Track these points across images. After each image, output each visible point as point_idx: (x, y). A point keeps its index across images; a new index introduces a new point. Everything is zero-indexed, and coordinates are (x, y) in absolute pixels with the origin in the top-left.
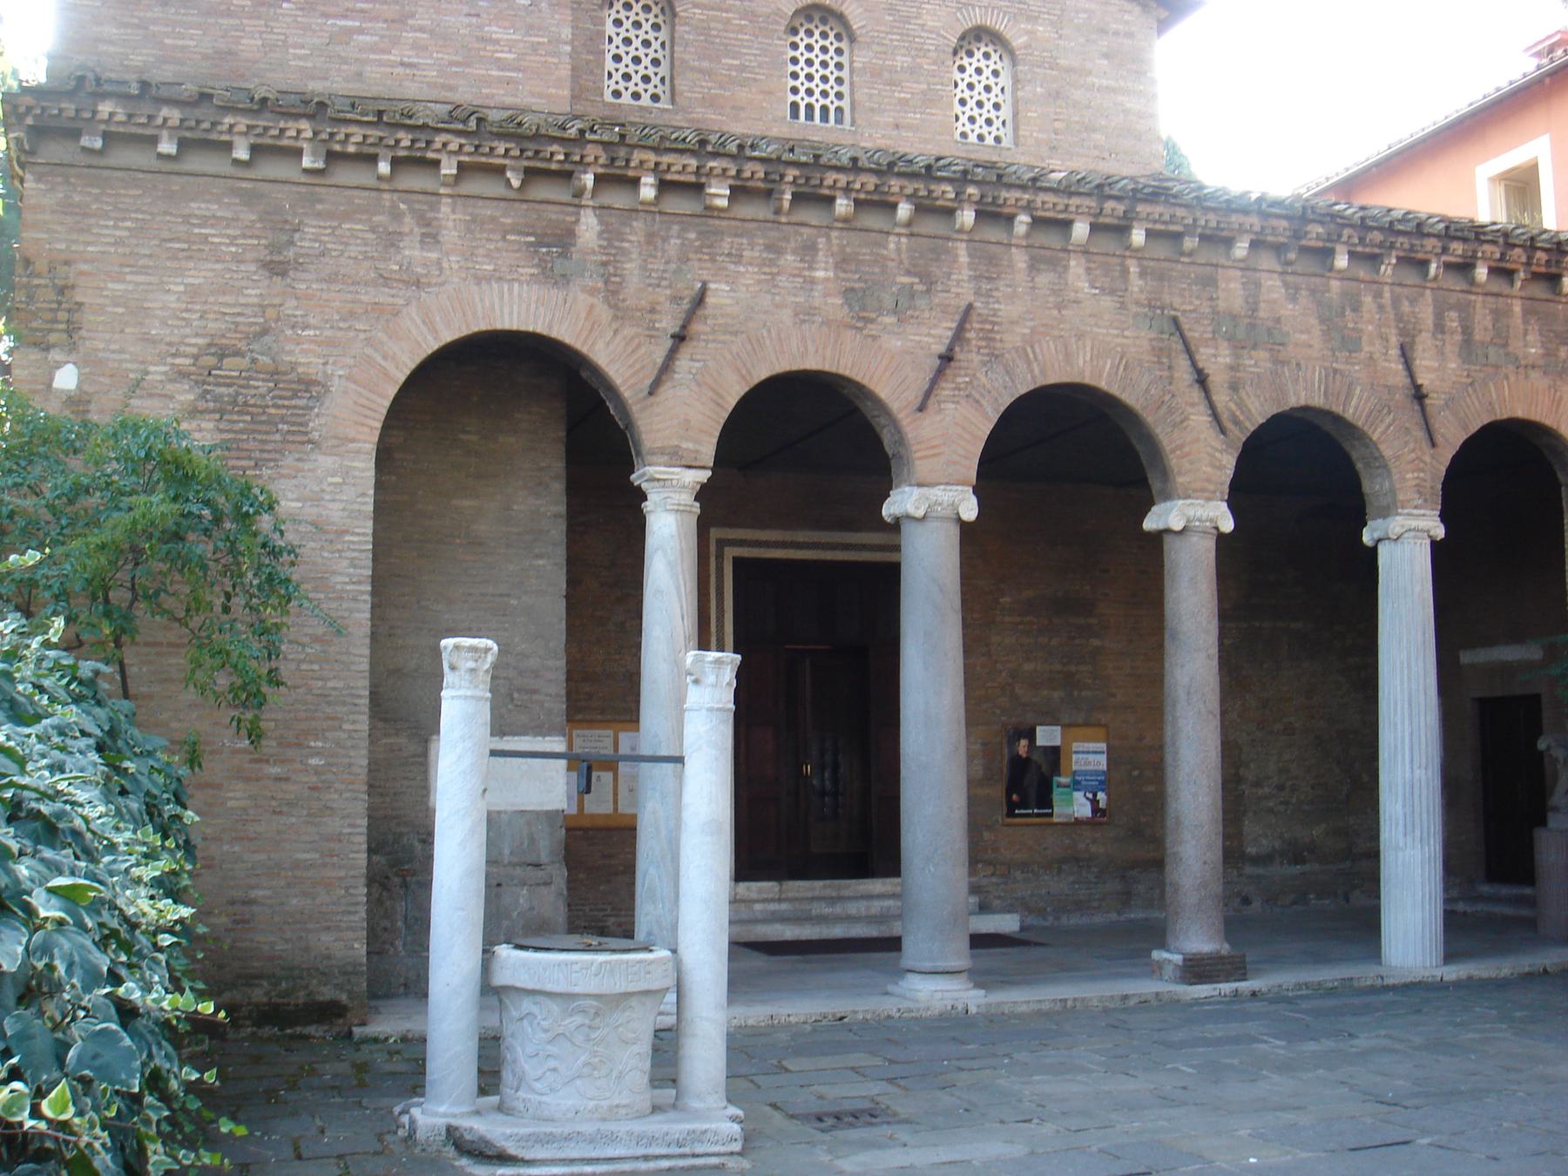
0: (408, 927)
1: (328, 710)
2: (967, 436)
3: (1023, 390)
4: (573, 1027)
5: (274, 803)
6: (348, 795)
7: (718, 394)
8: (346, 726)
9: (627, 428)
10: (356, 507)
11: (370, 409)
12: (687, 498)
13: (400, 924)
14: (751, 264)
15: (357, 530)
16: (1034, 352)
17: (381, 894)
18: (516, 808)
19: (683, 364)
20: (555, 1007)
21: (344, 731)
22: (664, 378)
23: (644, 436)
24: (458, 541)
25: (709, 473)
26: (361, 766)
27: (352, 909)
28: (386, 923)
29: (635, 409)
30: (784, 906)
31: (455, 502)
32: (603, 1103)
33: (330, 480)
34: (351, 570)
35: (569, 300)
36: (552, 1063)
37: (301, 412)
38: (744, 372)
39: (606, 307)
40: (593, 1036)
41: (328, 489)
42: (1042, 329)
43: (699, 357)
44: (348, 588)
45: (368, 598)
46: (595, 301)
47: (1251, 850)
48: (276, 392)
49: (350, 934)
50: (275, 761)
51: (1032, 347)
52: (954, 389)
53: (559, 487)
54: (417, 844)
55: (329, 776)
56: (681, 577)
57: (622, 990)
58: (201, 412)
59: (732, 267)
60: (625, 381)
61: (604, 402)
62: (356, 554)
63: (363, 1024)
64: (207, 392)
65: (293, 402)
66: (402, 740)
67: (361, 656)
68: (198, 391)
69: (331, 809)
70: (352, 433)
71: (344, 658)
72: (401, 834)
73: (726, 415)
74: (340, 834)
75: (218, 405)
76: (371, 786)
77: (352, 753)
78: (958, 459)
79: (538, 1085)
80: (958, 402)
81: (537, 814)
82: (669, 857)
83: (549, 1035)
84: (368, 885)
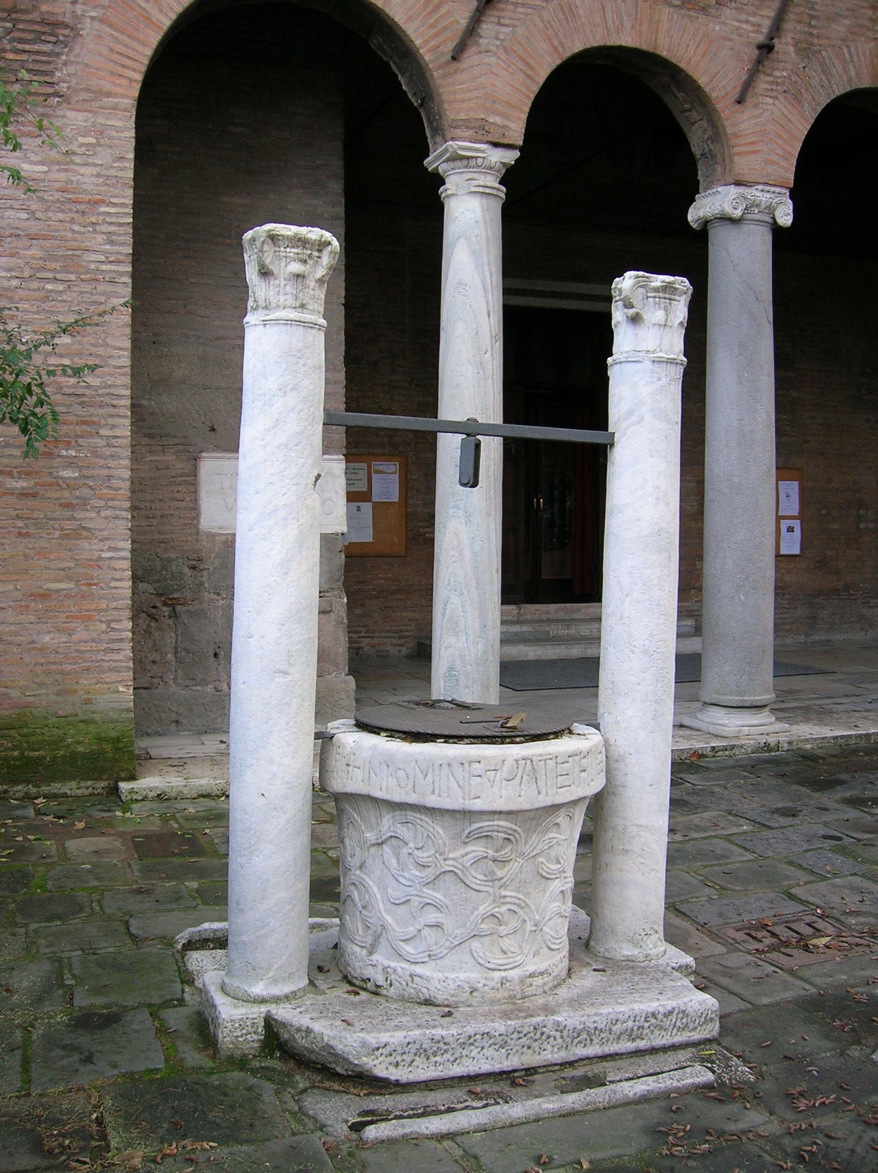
0: (179, 661)
1: (81, 411)
2: (785, 136)
3: (839, 91)
4: (468, 861)
5: (20, 523)
6: (108, 513)
7: (527, 64)
8: (103, 432)
9: (421, 105)
10: (113, 172)
11: (129, 57)
12: (492, 181)
13: (170, 656)
15: (113, 200)
16: (850, 52)
17: (148, 625)
20: (439, 830)
21: (101, 437)
23: (446, 106)
24: (228, 241)
25: (516, 154)
26: (124, 480)
27: (115, 646)
28: (156, 656)
29: (436, 74)
30: (525, 628)
32: (510, 974)
33: (81, 140)
34: (108, 247)
36: (432, 916)
37: (44, 59)
40: (499, 874)
41: (79, 151)
43: (506, 21)
44: (104, 267)
45: (128, 280)
48: (16, 34)
49: (114, 676)
50: (20, 473)
52: (772, 83)
55: (86, 492)
56: (487, 268)
57: (548, 802)
60: (426, 42)
61: (397, 76)
62: (112, 228)
63: (132, 778)
65: (36, 47)
66: (169, 458)
67: (121, 349)
69: (87, 529)
70: (107, 86)
71: (101, 351)
72: (169, 560)
74: (100, 558)
76: (134, 508)
77: (112, 464)
78: (775, 158)
79: (408, 949)
80: (776, 98)
82: (474, 583)
83: (430, 873)
84: (133, 618)
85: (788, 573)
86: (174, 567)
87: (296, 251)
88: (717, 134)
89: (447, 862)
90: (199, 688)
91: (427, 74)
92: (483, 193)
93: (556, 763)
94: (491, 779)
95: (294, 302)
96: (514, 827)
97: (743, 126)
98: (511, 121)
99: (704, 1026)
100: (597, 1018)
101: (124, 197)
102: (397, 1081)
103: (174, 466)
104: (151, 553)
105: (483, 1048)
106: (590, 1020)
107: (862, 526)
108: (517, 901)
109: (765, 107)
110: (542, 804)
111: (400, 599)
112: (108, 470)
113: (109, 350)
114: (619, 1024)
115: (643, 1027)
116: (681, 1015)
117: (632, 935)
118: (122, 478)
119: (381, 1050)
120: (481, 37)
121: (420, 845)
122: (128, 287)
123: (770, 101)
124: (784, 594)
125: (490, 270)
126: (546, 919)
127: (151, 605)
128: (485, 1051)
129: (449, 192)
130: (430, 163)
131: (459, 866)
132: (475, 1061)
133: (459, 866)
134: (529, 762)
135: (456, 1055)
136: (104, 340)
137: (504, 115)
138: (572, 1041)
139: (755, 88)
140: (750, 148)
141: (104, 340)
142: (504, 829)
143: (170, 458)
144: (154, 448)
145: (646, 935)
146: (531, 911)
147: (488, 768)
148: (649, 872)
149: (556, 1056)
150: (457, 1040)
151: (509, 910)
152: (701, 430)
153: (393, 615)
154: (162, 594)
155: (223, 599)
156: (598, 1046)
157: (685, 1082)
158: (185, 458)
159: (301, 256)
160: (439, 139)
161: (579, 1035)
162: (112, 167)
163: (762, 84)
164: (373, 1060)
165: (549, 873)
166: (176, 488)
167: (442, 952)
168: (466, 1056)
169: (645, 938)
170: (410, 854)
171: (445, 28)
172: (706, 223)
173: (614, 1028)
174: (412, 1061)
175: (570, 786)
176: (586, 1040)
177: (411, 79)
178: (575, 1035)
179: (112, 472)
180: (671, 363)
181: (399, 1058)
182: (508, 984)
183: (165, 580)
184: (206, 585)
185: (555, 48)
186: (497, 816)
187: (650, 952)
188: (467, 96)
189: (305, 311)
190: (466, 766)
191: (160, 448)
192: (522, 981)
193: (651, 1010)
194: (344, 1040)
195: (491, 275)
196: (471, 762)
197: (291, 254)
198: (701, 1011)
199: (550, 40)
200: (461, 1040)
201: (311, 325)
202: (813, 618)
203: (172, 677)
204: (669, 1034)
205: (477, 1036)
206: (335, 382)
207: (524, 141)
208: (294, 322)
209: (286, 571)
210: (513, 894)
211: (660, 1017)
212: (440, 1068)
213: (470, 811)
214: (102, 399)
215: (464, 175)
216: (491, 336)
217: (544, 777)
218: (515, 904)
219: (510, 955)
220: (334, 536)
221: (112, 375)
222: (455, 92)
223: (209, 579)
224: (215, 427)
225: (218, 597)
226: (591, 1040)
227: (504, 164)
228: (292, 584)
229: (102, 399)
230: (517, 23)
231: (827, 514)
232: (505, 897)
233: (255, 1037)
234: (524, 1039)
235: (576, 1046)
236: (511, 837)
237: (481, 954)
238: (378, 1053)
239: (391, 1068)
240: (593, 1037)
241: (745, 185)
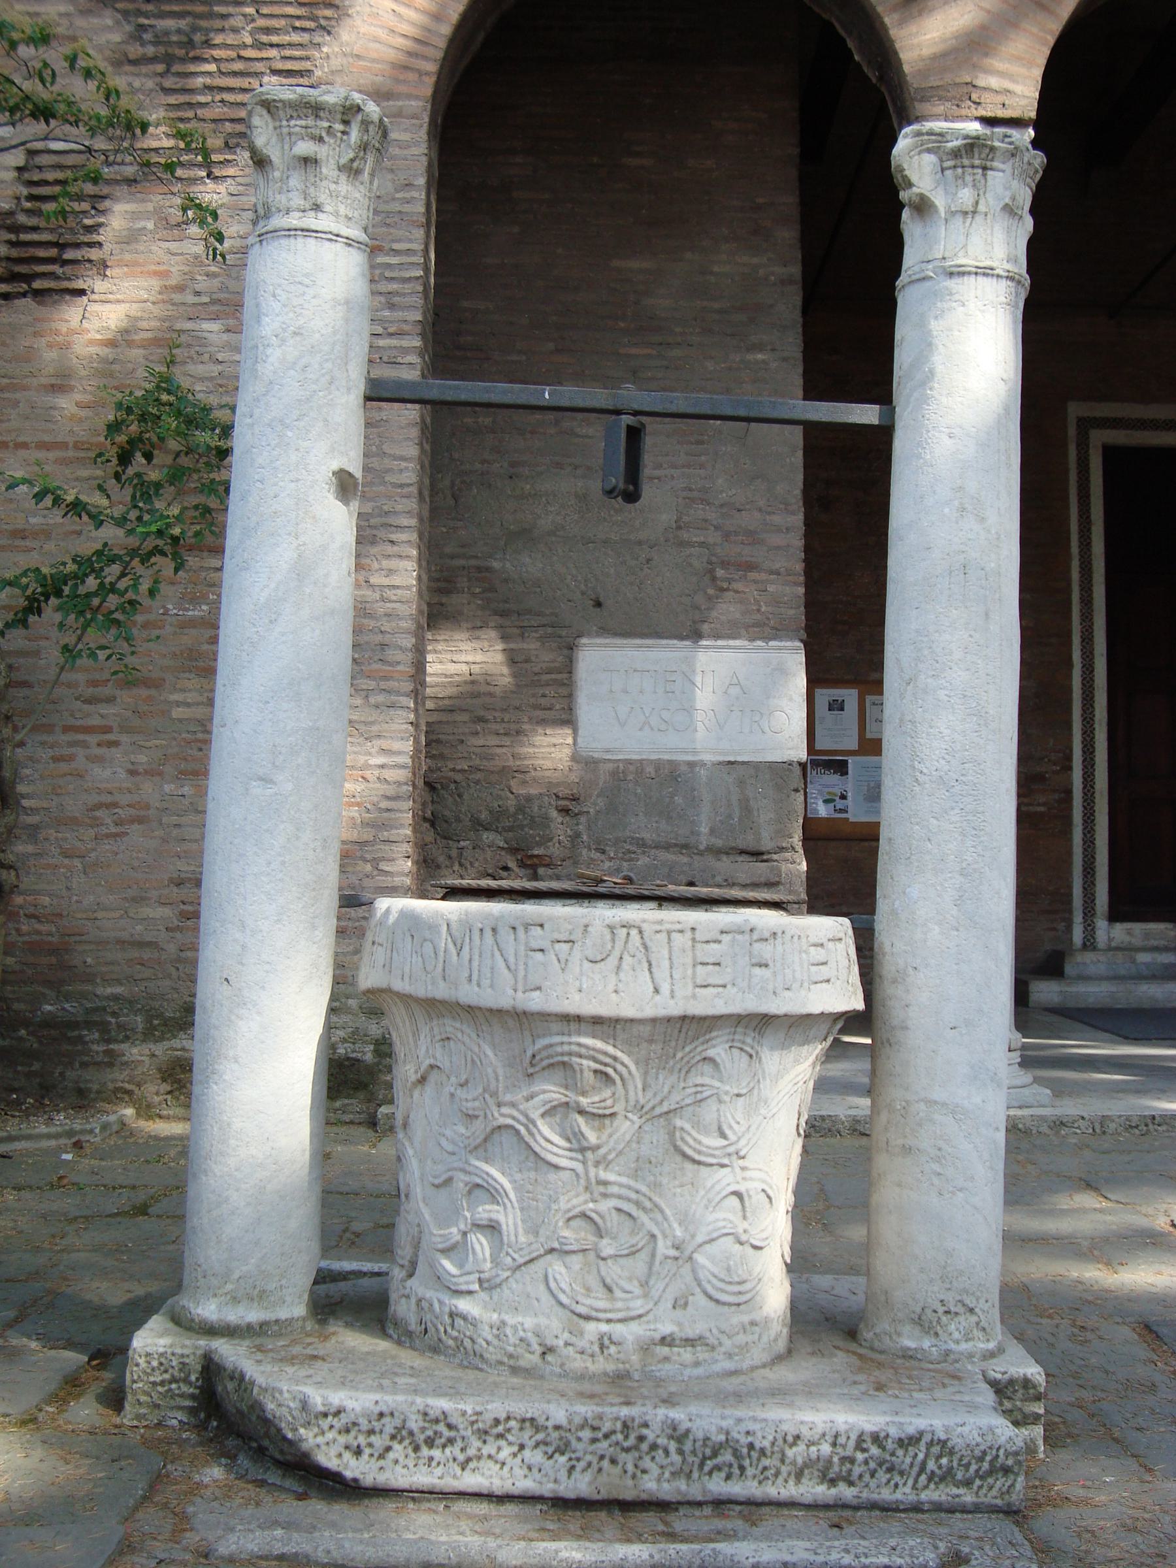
6: (381, 698)
10: (396, 206)
15: (396, 246)
18: (721, 758)
24: (622, 325)
31: (616, 263)
32: (618, 1330)
34: (387, 313)
53: (788, 235)
54: (554, 814)
58: (133, 62)
61: (844, 41)
62: (394, 286)
64: (142, 28)
68: (128, 28)
75: (162, 49)
77: (387, 627)
81: (756, 767)
87: (303, 123)
89: (504, 1110)
93: (694, 940)
94: (563, 957)
95: (302, 202)
96: (610, 1049)
98: (1017, 83)
99: (990, 1480)
100: (752, 1426)
101: (410, 241)
102: (355, 1480)
103: (537, 656)
104: (502, 786)
105: (522, 1447)
106: (739, 1428)
108: (633, 1196)
110: (661, 1012)
112: (380, 636)
113: (386, 461)
114: (801, 1447)
115: (852, 1461)
116: (936, 1450)
117: (918, 1310)
118: (401, 648)
119: (330, 1418)
122: (414, 369)
127: (500, 864)
128: (527, 1453)
131: (521, 1118)
132: (506, 1469)
133: (521, 1118)
134: (634, 932)
135: (471, 1452)
136: (379, 447)
138: (702, 1465)
141: (379, 447)
142: (591, 1052)
143: (532, 646)
144: (508, 630)
145: (946, 1312)
146: (666, 1219)
147: (557, 936)
148: (953, 1193)
149: (666, 1485)
150: (473, 1423)
151: (619, 1210)
154: (517, 850)
155: (611, 859)
156: (755, 1483)
157: (874, 1560)
158: (554, 645)
159: (313, 130)
161: (715, 1454)
162: (394, 199)
164: (315, 1436)
165: (699, 1152)
167: (498, 1275)
168: (490, 1457)
169: (944, 1319)
173: (790, 1453)
174: (388, 1449)
175: (724, 986)
176: (731, 1466)
178: (708, 1452)
179: (387, 638)
180: (984, 274)
181: (362, 1440)
182: (613, 1349)
183: (522, 827)
184: (585, 838)
186: (574, 1026)
187: (952, 1346)
189: (320, 215)
190: (521, 932)
192: (646, 1348)
193: (869, 1427)
194: (277, 1395)
196: (527, 926)
197: (297, 129)
198: (982, 1448)
200: (481, 1425)
201: (330, 236)
204: (910, 1482)
205: (512, 1423)
206: (787, 529)
208: (299, 233)
209: (274, 616)
210: (624, 1180)
211: (890, 1445)
212: (438, 1471)
214: (375, 532)
217: (666, 963)
218: (629, 1200)
219: (618, 1294)
220: (785, 766)
221: (390, 498)
223: (589, 828)
224: (601, 600)
225: (603, 857)
226: (742, 1469)
228: (284, 638)
229: (375, 532)
232: (605, 1183)
233: (185, 1389)
234: (604, 1444)
235: (710, 1473)
236: (610, 1071)
237: (563, 1285)
238: (325, 1423)
239: (347, 1455)
240: (747, 1463)
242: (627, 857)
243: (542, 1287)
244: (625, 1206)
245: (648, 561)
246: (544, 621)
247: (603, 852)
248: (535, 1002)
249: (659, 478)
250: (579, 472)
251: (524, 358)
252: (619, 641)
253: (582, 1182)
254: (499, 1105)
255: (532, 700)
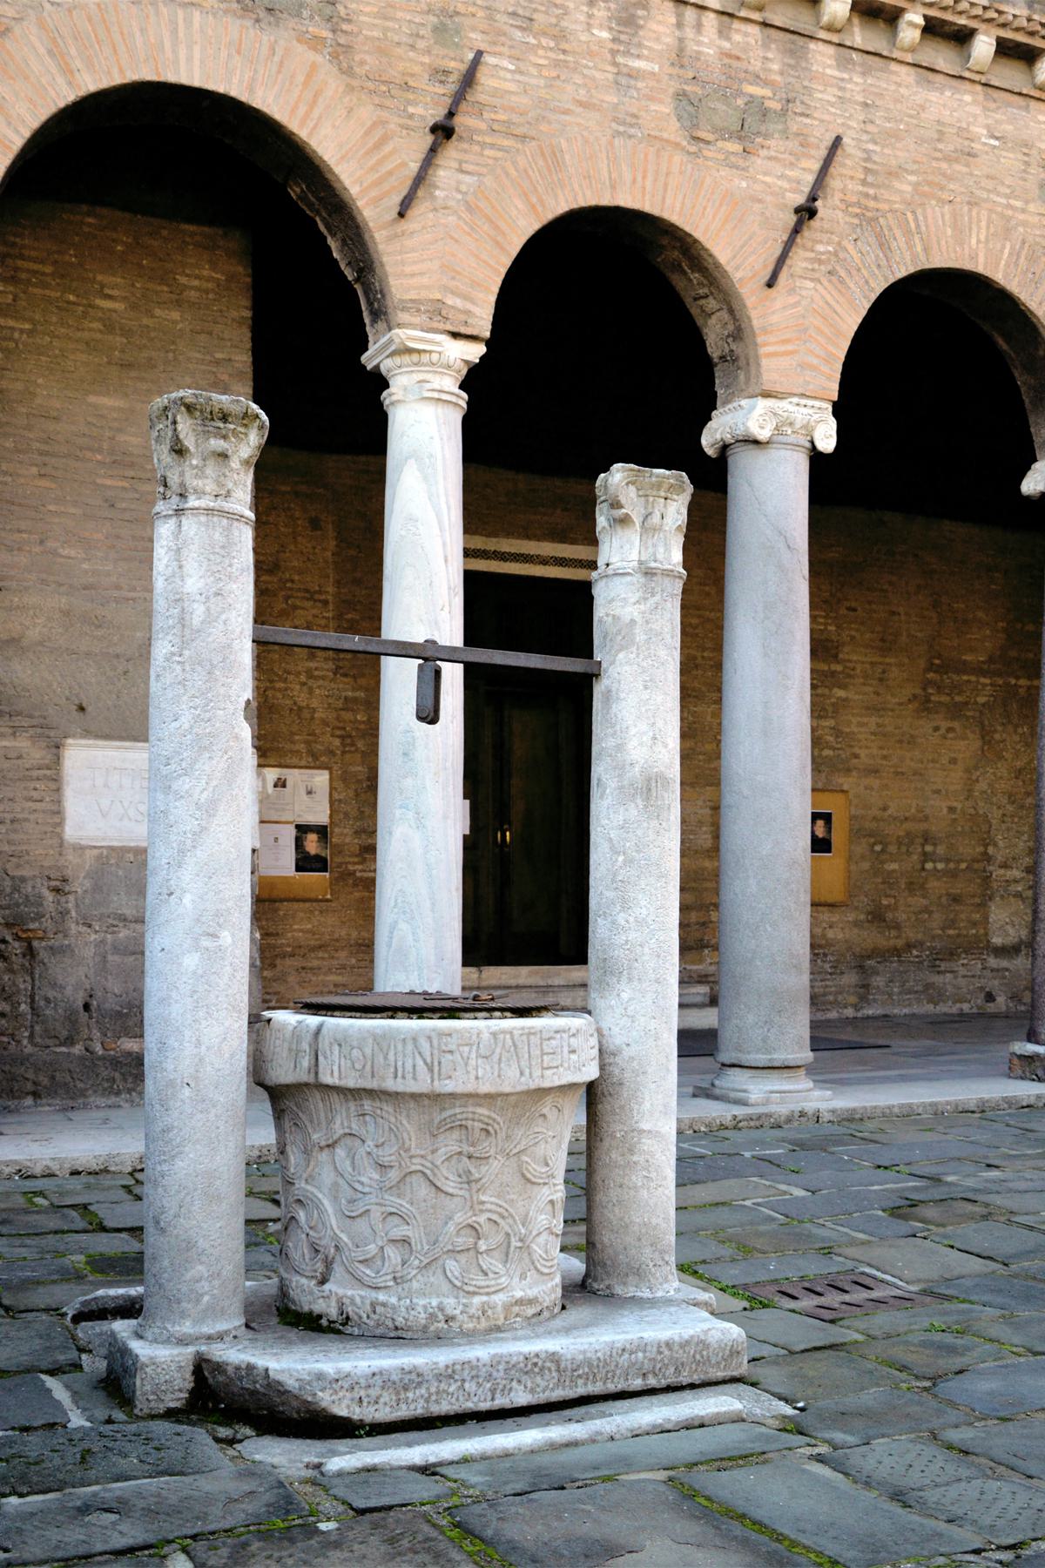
3: (901, 273)
7: (497, 228)
9: (357, 280)
12: (450, 384)
14: (545, 34)
19: (444, 174)
22: (420, 193)
25: (481, 349)
31: (92, 399)
35: (279, 52)
38: (534, 200)
39: (335, 70)
42: (926, 188)
43: (470, 168)
46: (319, 59)
47: (997, 940)
51: (913, 212)
59: (518, 34)
60: (363, 191)
66: (22, 743)
72: (23, 880)
73: (508, 262)
78: (815, 361)
85: (831, 927)
86: (30, 889)
88: (739, 332)
89: (414, 1161)
90: (64, 1049)
91: (367, 237)
92: (439, 400)
94: (465, 1055)
97: (775, 319)
107: (929, 866)
109: (804, 293)
111: (323, 958)
120: (437, 187)
121: (381, 1140)
123: (810, 284)
124: (825, 955)
125: (447, 502)
126: (534, 1233)
129: (394, 398)
130: (370, 359)
131: (429, 1165)
133: (429, 1165)
134: (508, 1036)
137: (465, 297)
139: (790, 267)
140: (783, 348)
143: (24, 744)
151: (490, 1219)
152: (717, 646)
153: (314, 979)
154: (13, 925)
155: (96, 932)
160: (381, 325)
163: (799, 260)
166: (32, 785)
170: (369, 1153)
171: (390, 173)
172: (724, 448)
177: (344, 241)
181: (362, 1393)
183: (18, 905)
184: (73, 914)
185: (533, 207)
188: (415, 268)
191: (10, 731)
192: (507, 1307)
195: (449, 508)
199: (525, 194)
202: (863, 986)
203: (26, 1034)
207: (492, 332)
210: (493, 1199)
213: (439, 1095)
215: (414, 375)
216: (449, 588)
217: (526, 1056)
219: (491, 1275)
222: (403, 263)
223: (77, 906)
227: (466, 362)
230: (484, 170)
231: (883, 851)
232: (483, 1203)
236: (490, 1128)
241: (775, 397)
242: (110, 930)
243: (442, 1277)
244: (495, 1217)
245: (125, 673)
246: (35, 722)
247: (90, 926)
248: (449, 1086)
249: (134, 599)
250: (62, 589)
251: (10, 479)
252: (101, 743)
253: (469, 1203)
254: (411, 1157)
255: (25, 793)
